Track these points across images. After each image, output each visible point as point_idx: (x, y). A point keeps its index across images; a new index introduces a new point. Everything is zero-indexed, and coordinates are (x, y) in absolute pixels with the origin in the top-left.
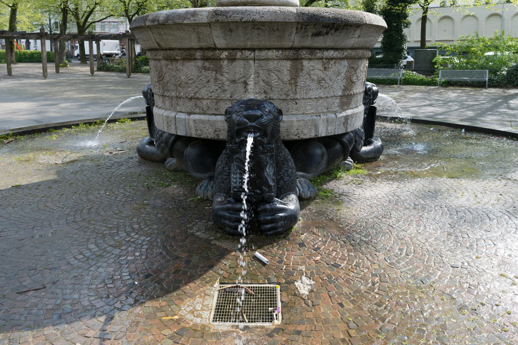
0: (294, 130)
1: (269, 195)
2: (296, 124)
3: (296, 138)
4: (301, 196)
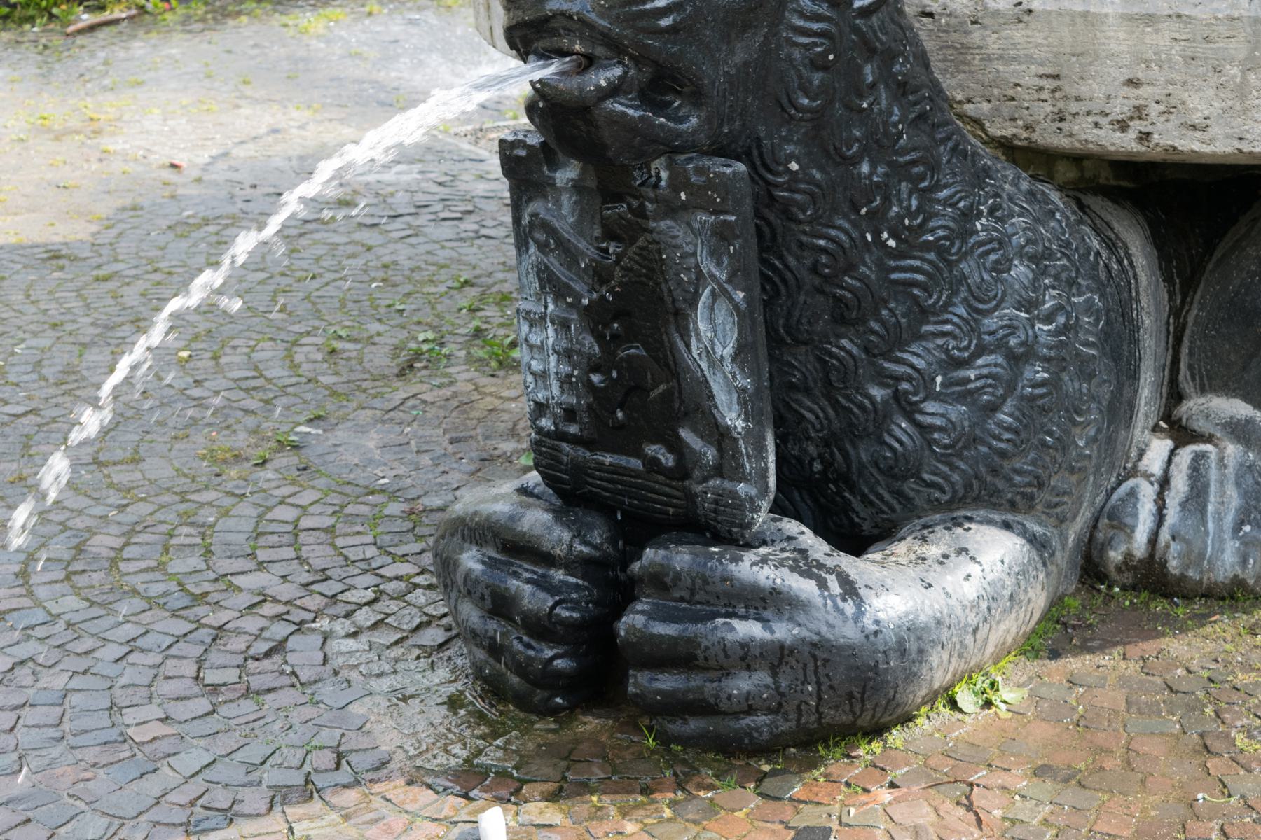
0: (1102, 87)
1: (720, 495)
2: (1117, 40)
3: (1125, 143)
4: (1164, 564)
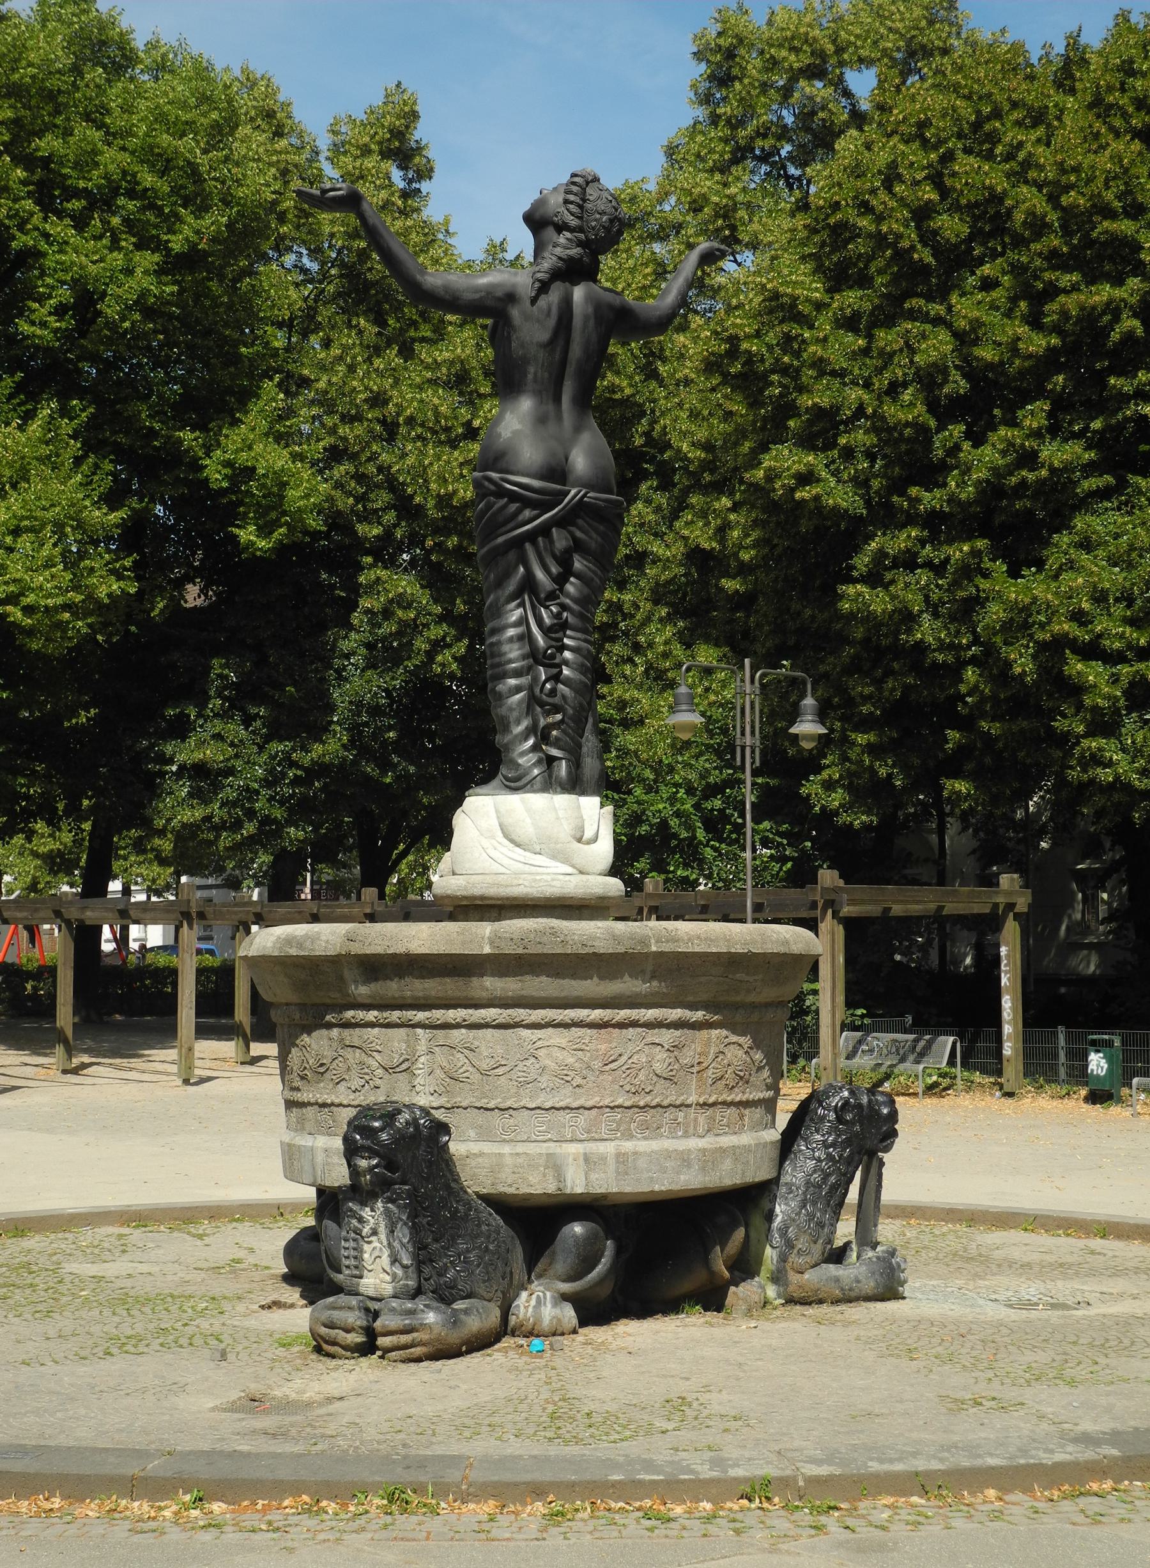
2: (509, 1161)
